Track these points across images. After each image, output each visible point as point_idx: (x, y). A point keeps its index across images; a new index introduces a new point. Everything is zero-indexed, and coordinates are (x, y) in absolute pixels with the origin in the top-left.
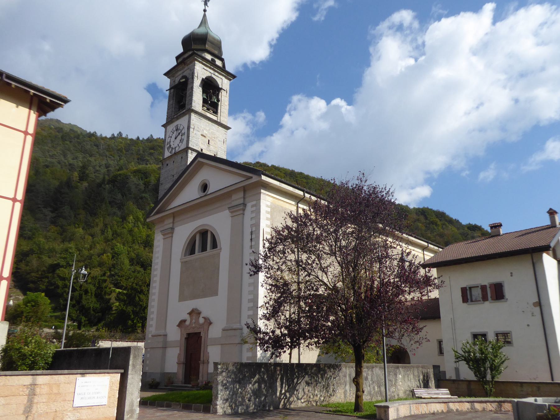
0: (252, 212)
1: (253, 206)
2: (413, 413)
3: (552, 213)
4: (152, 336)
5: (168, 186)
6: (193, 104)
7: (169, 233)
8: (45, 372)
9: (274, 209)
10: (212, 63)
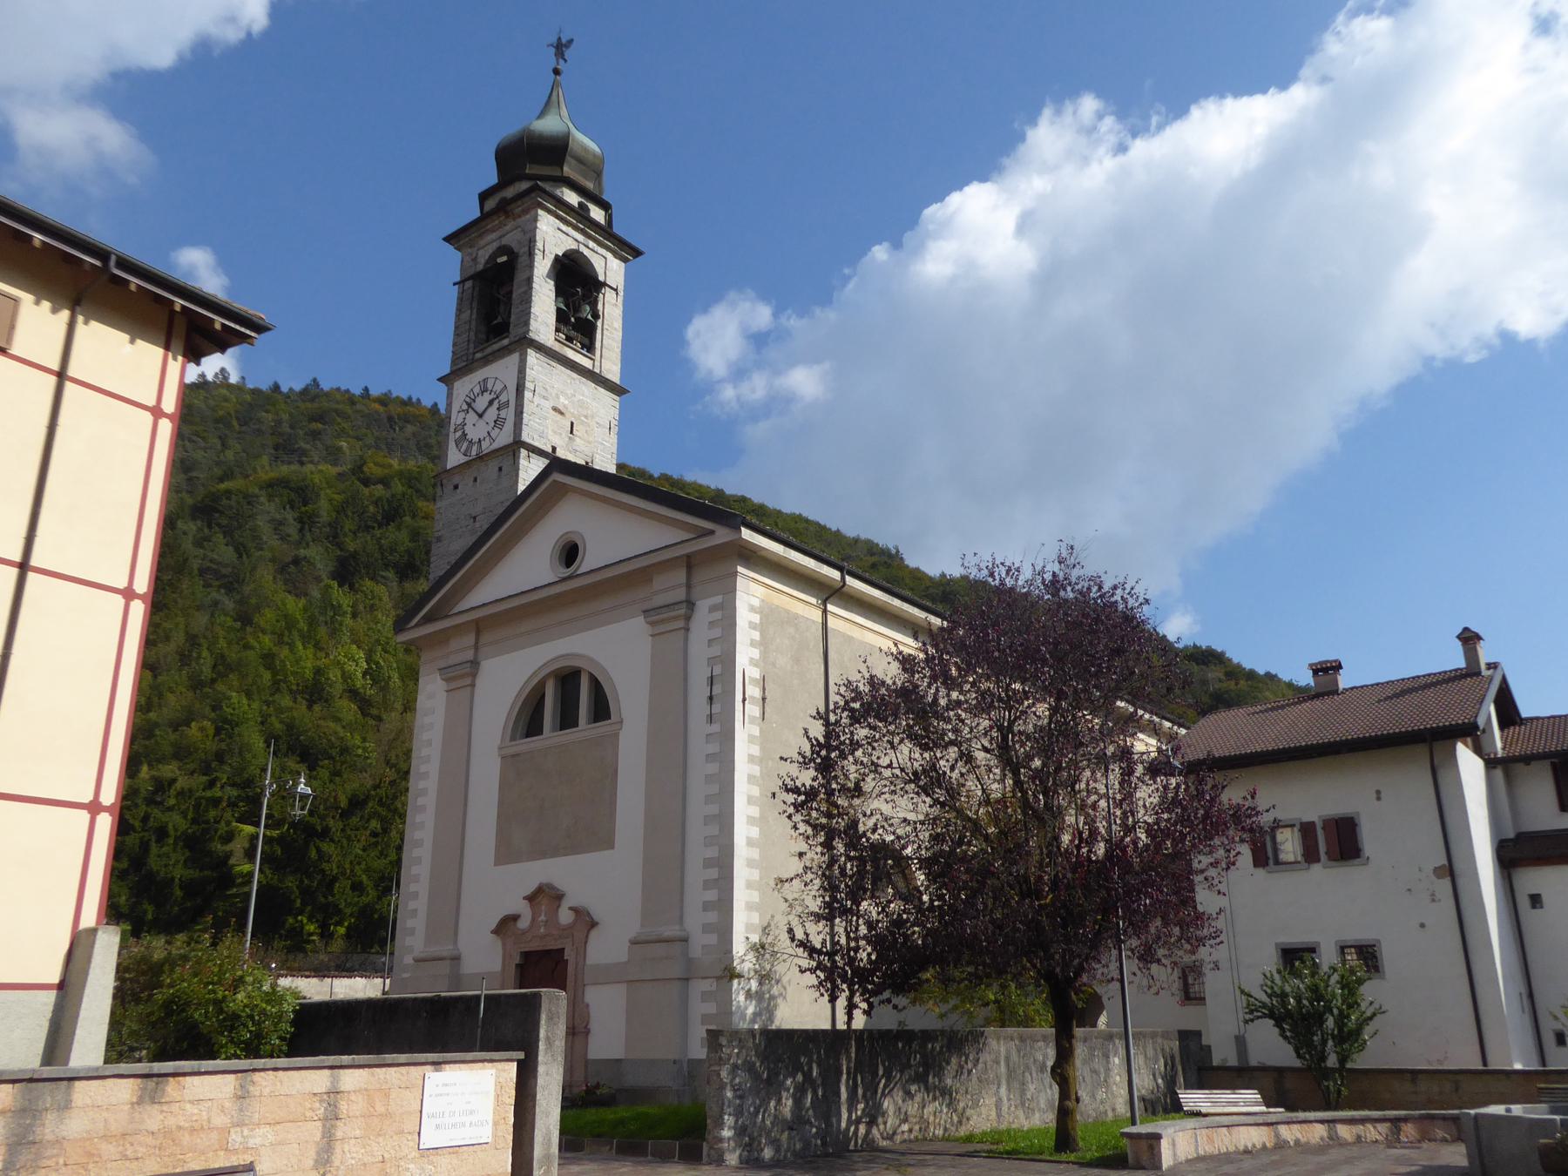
0: (712, 624)
1: (713, 609)
2: (1202, 1153)
3: (1469, 639)
4: (417, 960)
5: (459, 545)
6: (533, 325)
7: (464, 676)
8: (282, 1062)
9: (770, 618)
10: (581, 214)
